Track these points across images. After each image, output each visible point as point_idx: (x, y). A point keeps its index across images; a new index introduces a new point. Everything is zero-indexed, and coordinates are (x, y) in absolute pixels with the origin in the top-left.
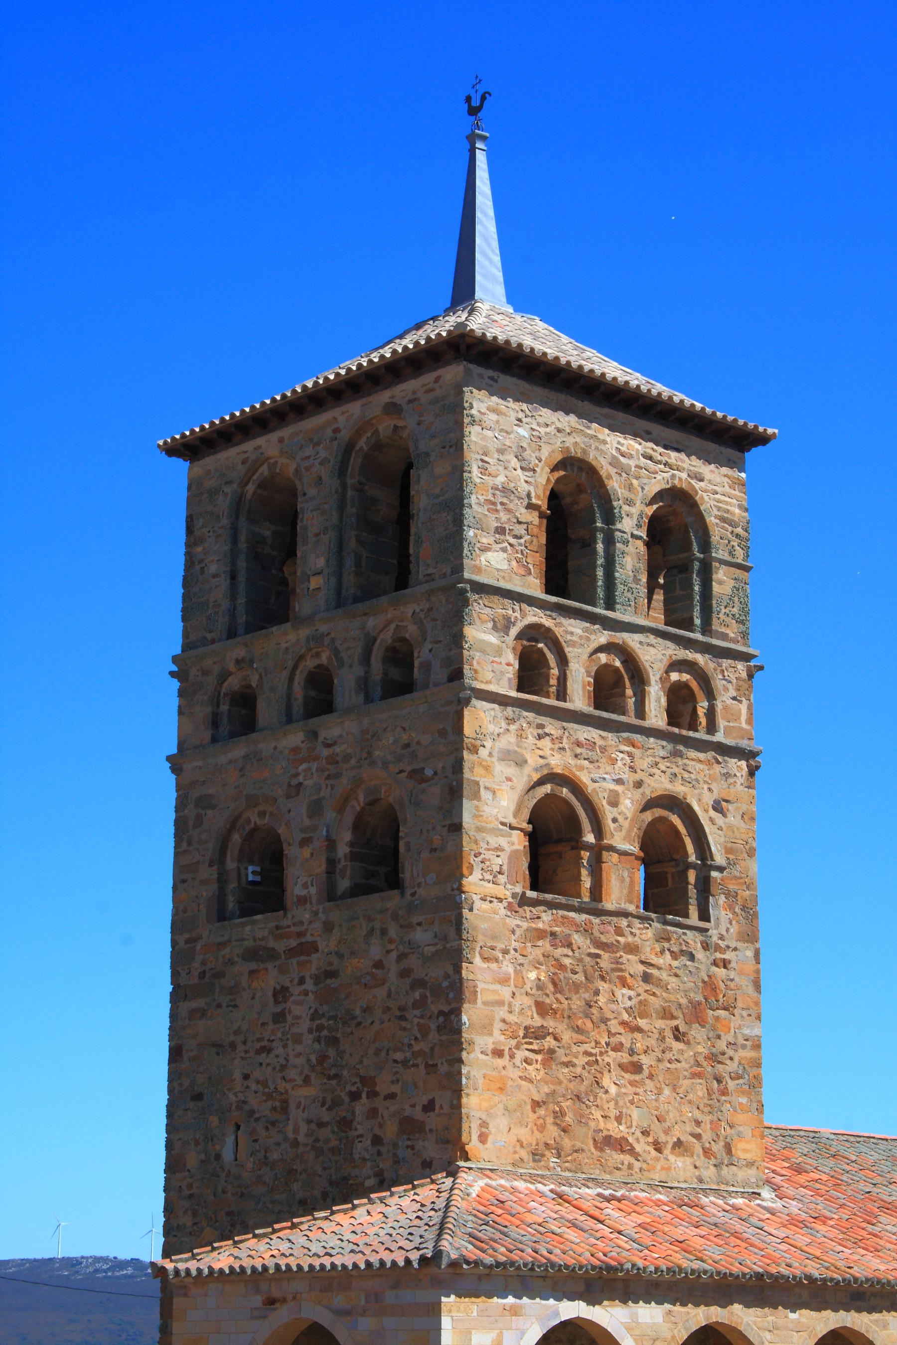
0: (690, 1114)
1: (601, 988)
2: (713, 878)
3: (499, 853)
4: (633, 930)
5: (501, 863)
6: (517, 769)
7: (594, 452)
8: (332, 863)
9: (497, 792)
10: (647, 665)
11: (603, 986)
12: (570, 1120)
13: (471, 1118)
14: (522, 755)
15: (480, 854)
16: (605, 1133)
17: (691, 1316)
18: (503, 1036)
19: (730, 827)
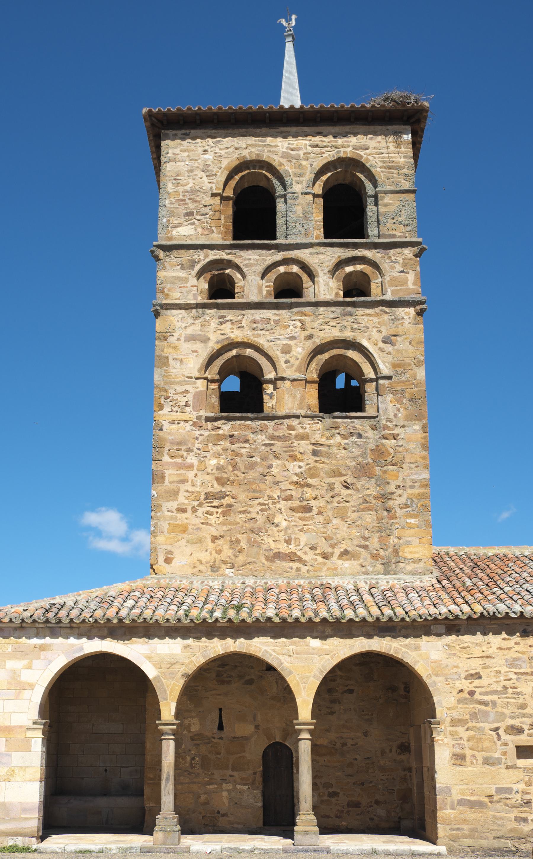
0: (358, 534)
1: (273, 464)
2: (381, 384)
3: (185, 395)
4: (304, 426)
5: (187, 400)
6: (202, 345)
7: (267, 154)
9: (184, 360)
10: (316, 266)
11: (276, 463)
12: (243, 545)
13: (159, 550)
14: (205, 336)
15: (169, 397)
16: (275, 551)
17: (209, 648)
18: (187, 500)
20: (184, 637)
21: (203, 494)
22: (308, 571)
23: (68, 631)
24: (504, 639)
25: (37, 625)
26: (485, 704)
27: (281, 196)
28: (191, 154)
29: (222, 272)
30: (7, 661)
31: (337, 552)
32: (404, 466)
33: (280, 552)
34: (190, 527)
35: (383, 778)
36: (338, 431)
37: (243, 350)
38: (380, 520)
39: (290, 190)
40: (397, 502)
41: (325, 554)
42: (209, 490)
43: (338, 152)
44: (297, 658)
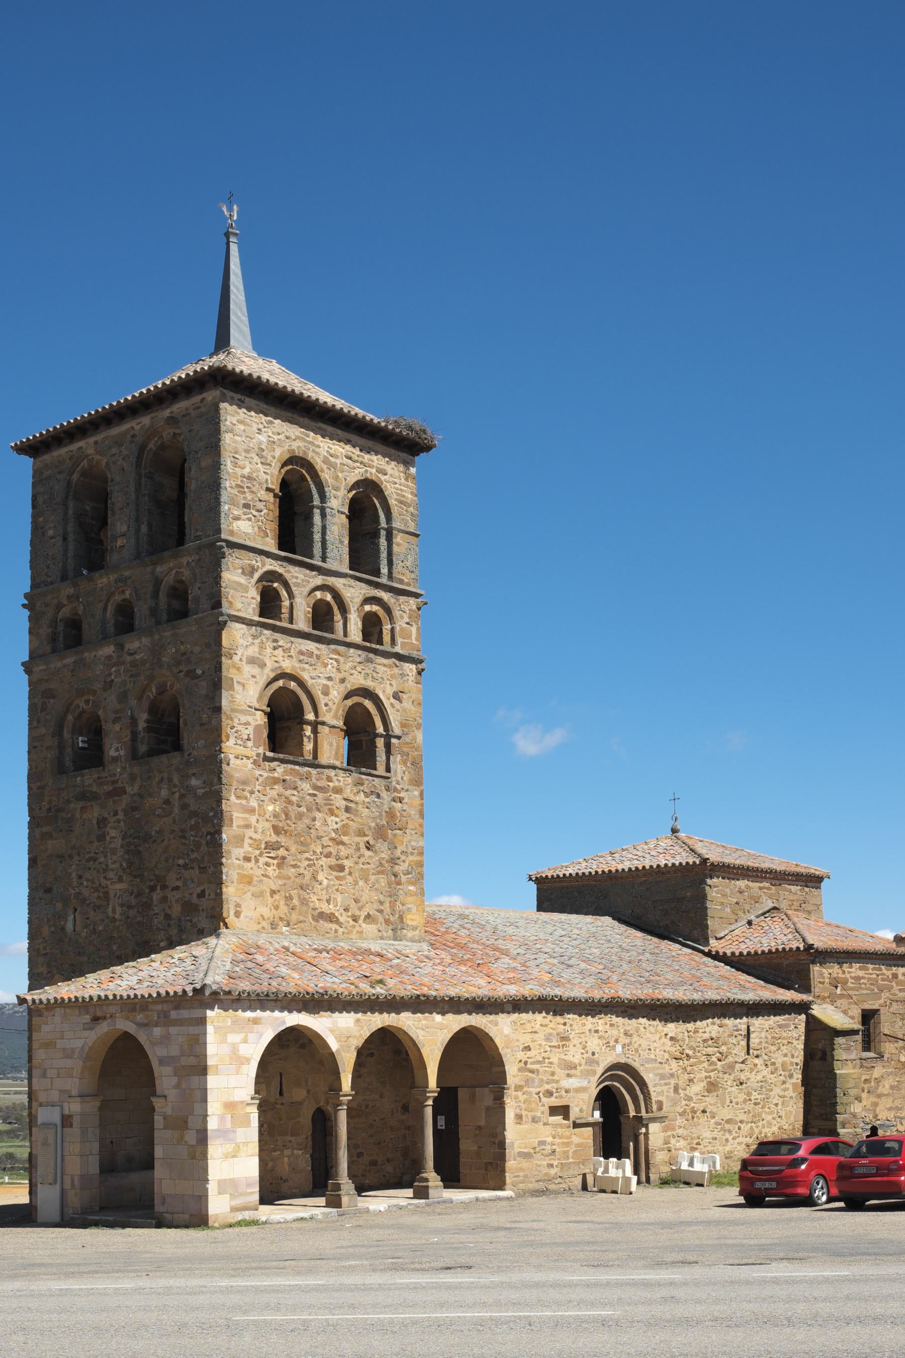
8: (134, 734)
11: (319, 815)
13: (230, 902)
16: (319, 910)
19: (404, 710)
20: (356, 1012)
21: (263, 842)
22: (343, 933)
23: (273, 1004)
24: (544, 1017)
25: (260, 998)
26: (532, 1071)
27: (318, 508)
28: (247, 428)
29: (270, 584)
30: (228, 1035)
31: (363, 914)
32: (407, 831)
33: (323, 912)
34: (255, 879)
35: (392, 1137)
36: (362, 788)
37: (288, 682)
38: (389, 884)
39: (329, 504)
40: (402, 868)
41: (355, 916)
42: (268, 839)
43: (366, 471)
44: (427, 1032)
